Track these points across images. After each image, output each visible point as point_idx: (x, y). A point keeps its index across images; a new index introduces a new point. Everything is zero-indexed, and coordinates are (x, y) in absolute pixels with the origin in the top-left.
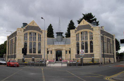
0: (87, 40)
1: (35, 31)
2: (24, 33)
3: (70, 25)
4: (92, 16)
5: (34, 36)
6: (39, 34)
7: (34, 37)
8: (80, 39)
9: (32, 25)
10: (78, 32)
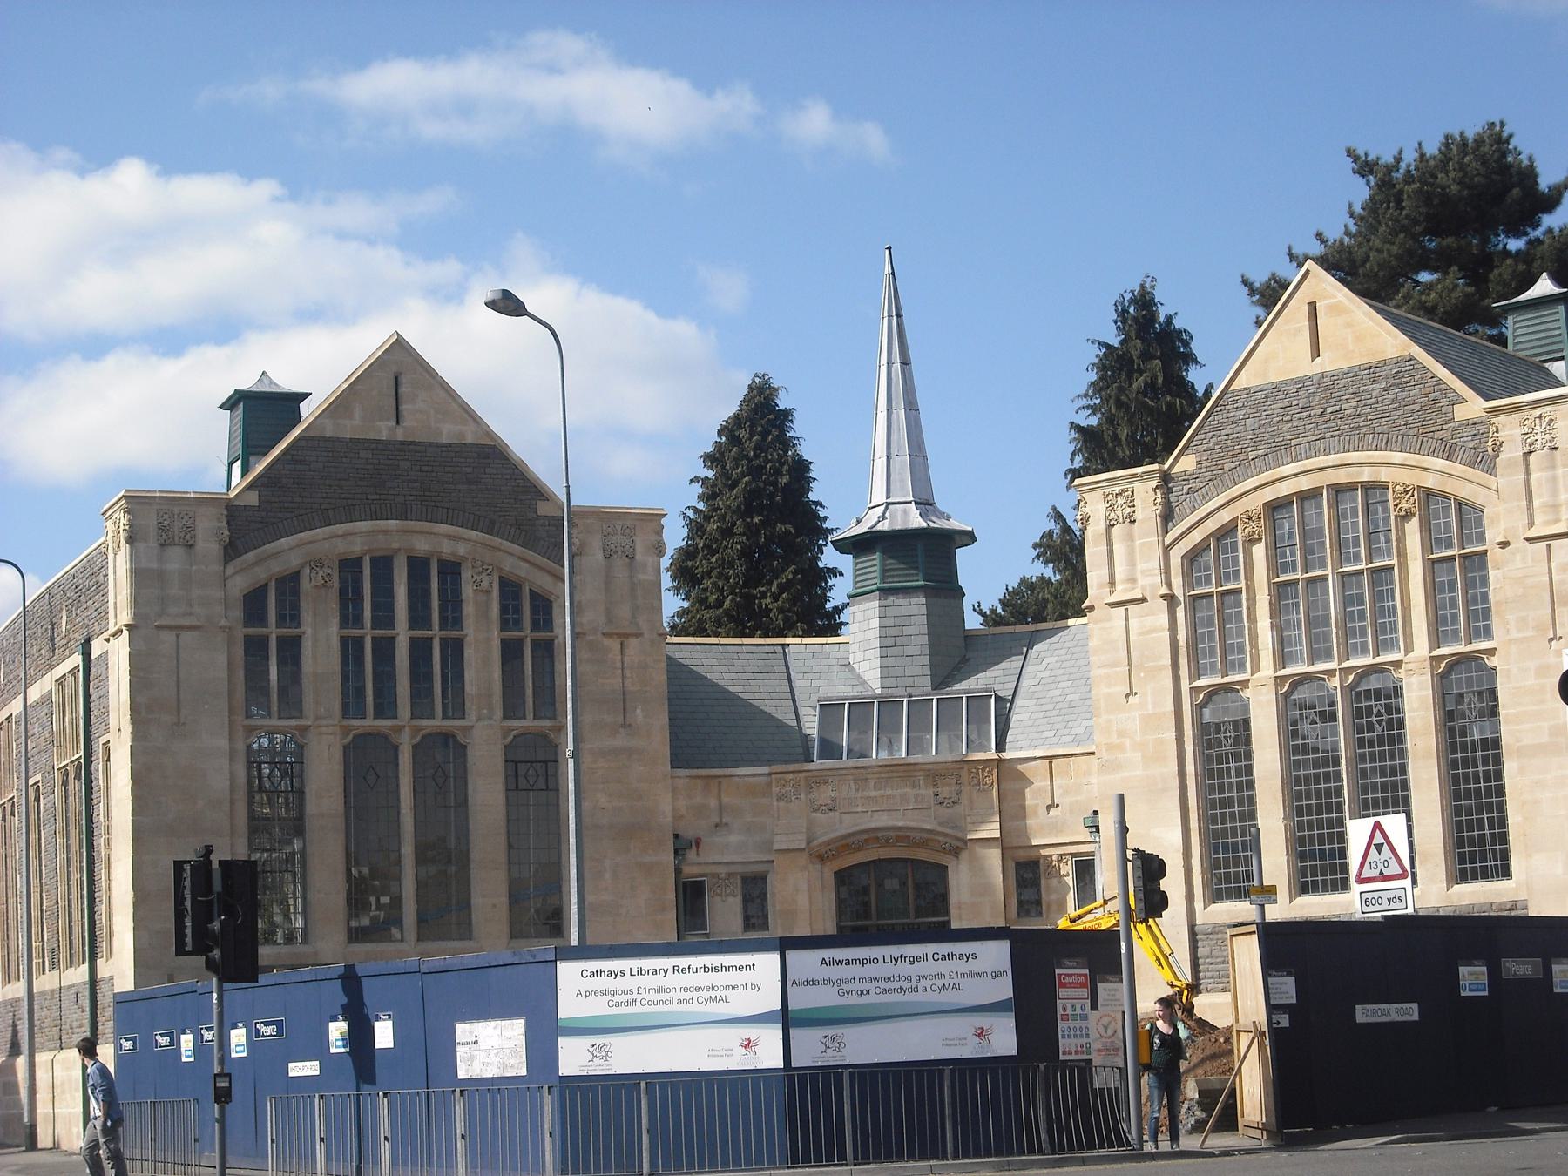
1: (440, 539)
2: (240, 584)
3: (1115, 367)
4: (1529, 174)
5: (418, 617)
6: (510, 590)
7: (420, 650)
9: (384, 430)
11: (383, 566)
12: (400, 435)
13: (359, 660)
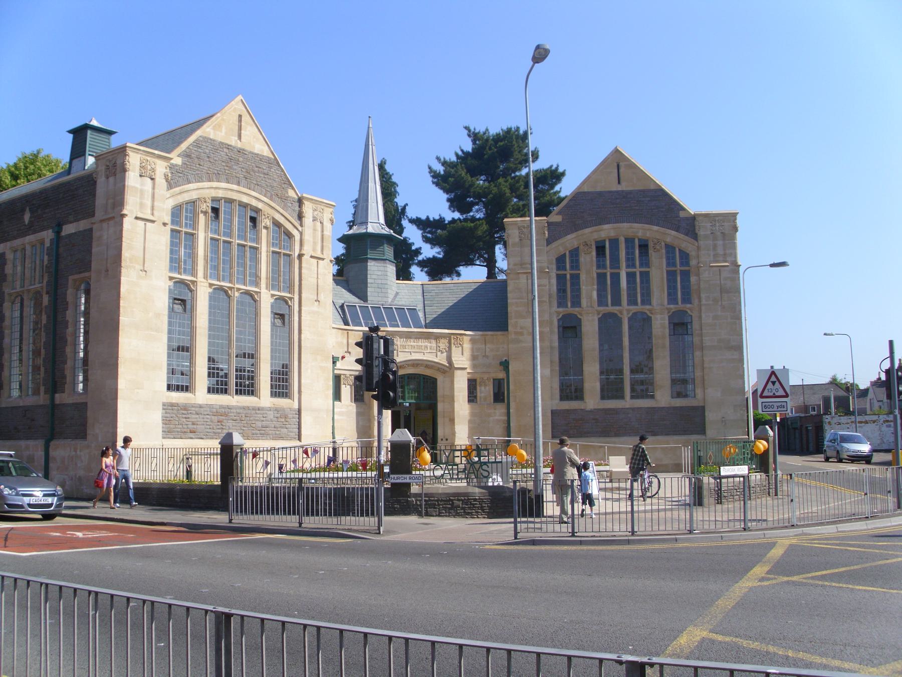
0: (573, 305)
8: (589, 291)
10: (570, 241)
11: (614, 242)
12: (239, 145)
13: (635, 282)
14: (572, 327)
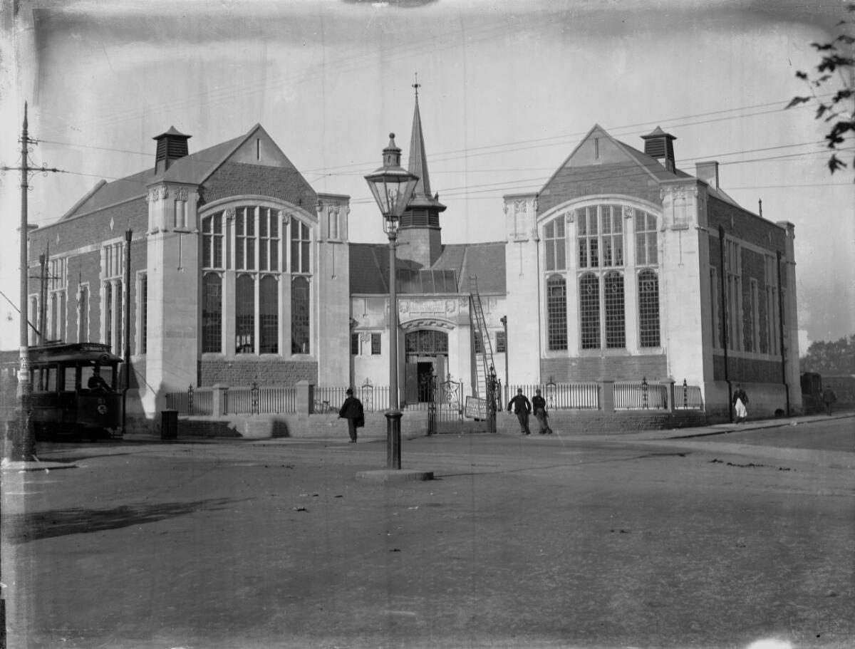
14: (711, 272)
